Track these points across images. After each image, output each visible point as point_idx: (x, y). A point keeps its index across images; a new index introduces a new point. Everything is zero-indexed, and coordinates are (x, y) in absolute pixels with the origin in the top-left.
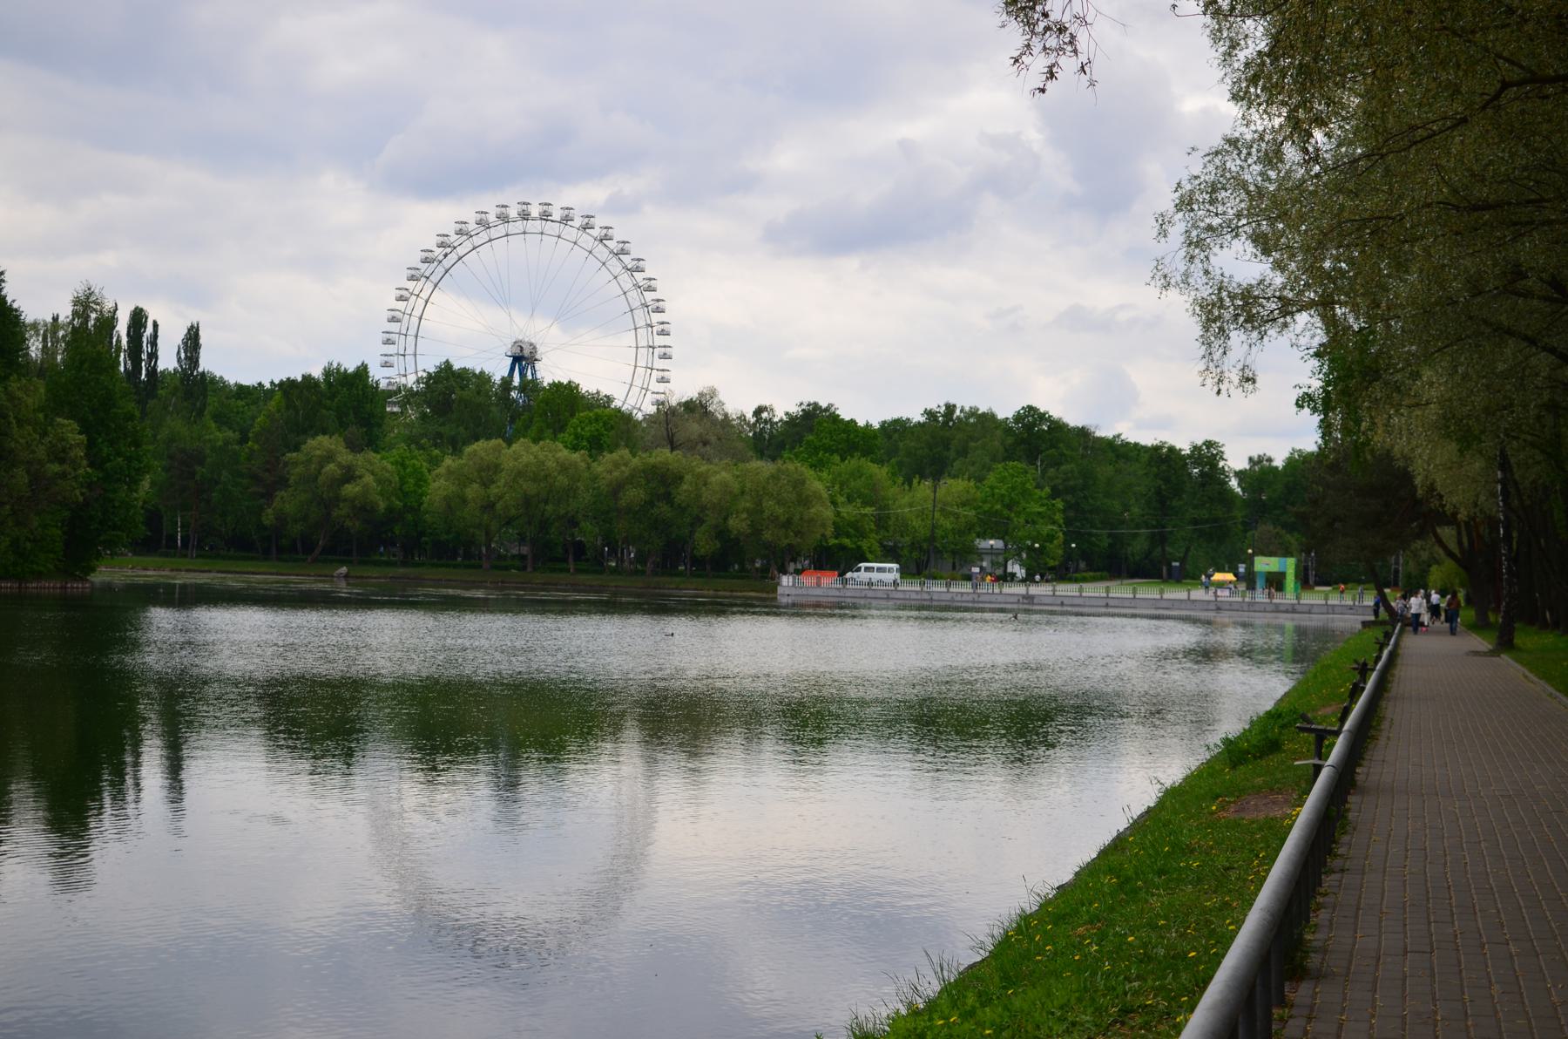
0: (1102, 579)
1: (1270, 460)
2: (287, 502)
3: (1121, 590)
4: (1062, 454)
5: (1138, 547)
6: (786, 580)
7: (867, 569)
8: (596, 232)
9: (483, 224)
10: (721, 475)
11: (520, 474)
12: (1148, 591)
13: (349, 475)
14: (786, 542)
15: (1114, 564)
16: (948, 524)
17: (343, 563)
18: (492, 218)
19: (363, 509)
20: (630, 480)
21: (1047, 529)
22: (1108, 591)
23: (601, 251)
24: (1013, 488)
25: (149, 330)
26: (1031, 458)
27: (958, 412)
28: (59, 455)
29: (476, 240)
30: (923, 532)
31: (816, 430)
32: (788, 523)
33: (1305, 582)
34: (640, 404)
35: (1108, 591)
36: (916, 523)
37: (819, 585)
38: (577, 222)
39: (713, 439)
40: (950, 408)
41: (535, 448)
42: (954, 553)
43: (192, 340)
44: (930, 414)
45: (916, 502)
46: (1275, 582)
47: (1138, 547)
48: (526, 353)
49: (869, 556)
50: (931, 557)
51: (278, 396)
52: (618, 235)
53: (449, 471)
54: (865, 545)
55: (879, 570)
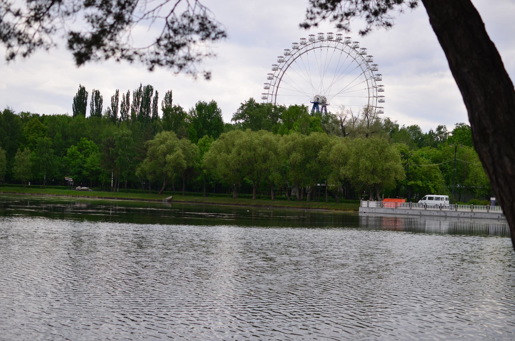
2: (146, 165)
6: (364, 204)
7: (430, 198)
9: (312, 41)
10: (339, 143)
11: (241, 147)
14: (372, 182)
16: (256, 141)
17: (170, 194)
18: (316, 38)
25: (154, 95)
29: (309, 48)
32: (374, 172)
43: (169, 97)
49: (433, 191)
52: (361, 45)
54: (430, 185)
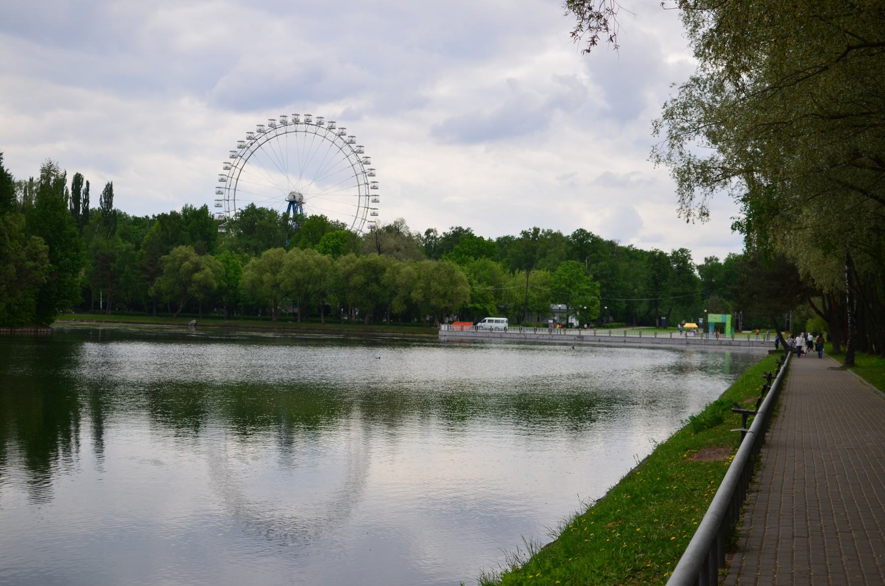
0: (622, 326)
1: (717, 259)
2: (162, 283)
3: (633, 333)
4: (599, 256)
5: (642, 308)
6: (444, 327)
7: (489, 321)
8: (336, 131)
9: (273, 126)
10: (407, 268)
11: (293, 267)
12: (648, 334)
13: (197, 268)
14: (444, 305)
15: (629, 318)
16: (535, 295)
17: (193, 317)
18: (278, 123)
19: (205, 287)
20: (356, 271)
21: (591, 298)
22: (625, 333)
23: (339, 142)
24: (572, 275)
25: (84, 186)
26: (582, 258)
27: (541, 233)
28: (34, 257)
29: (269, 136)
30: (521, 300)
31: (460, 243)
32: (445, 295)
33: (736, 328)
34: (361, 228)
35: (625, 333)
36: (517, 295)
37: (462, 330)
38: (326, 125)
39: (402, 247)
40: (536, 230)
41: (302, 253)
42: (538, 312)
43: (109, 192)
44: (525, 233)
45: (517, 283)
46: (720, 328)
47: (642, 308)
48: (297, 199)
49: (491, 314)
50: (525, 314)
51: (157, 223)
53: (254, 266)
54: (488, 307)
55: (496, 321)
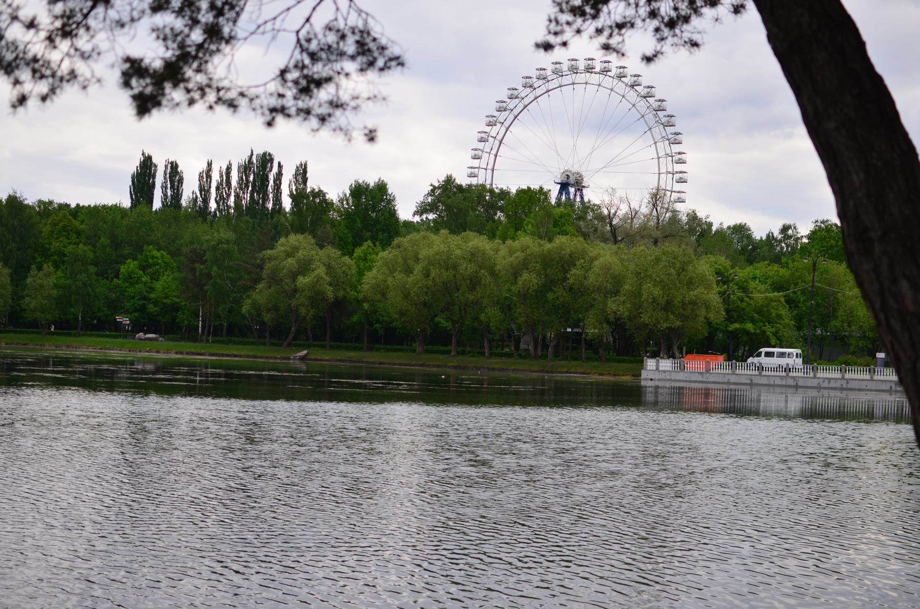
2: (261, 294)
6: (651, 364)
7: (768, 354)
9: (558, 73)
10: (605, 255)
11: (431, 263)
14: (665, 325)
16: (458, 252)
17: (303, 347)
18: (565, 68)
25: (275, 169)
29: (551, 85)
32: (668, 307)
43: (302, 173)
49: (773, 341)
54: (769, 330)
